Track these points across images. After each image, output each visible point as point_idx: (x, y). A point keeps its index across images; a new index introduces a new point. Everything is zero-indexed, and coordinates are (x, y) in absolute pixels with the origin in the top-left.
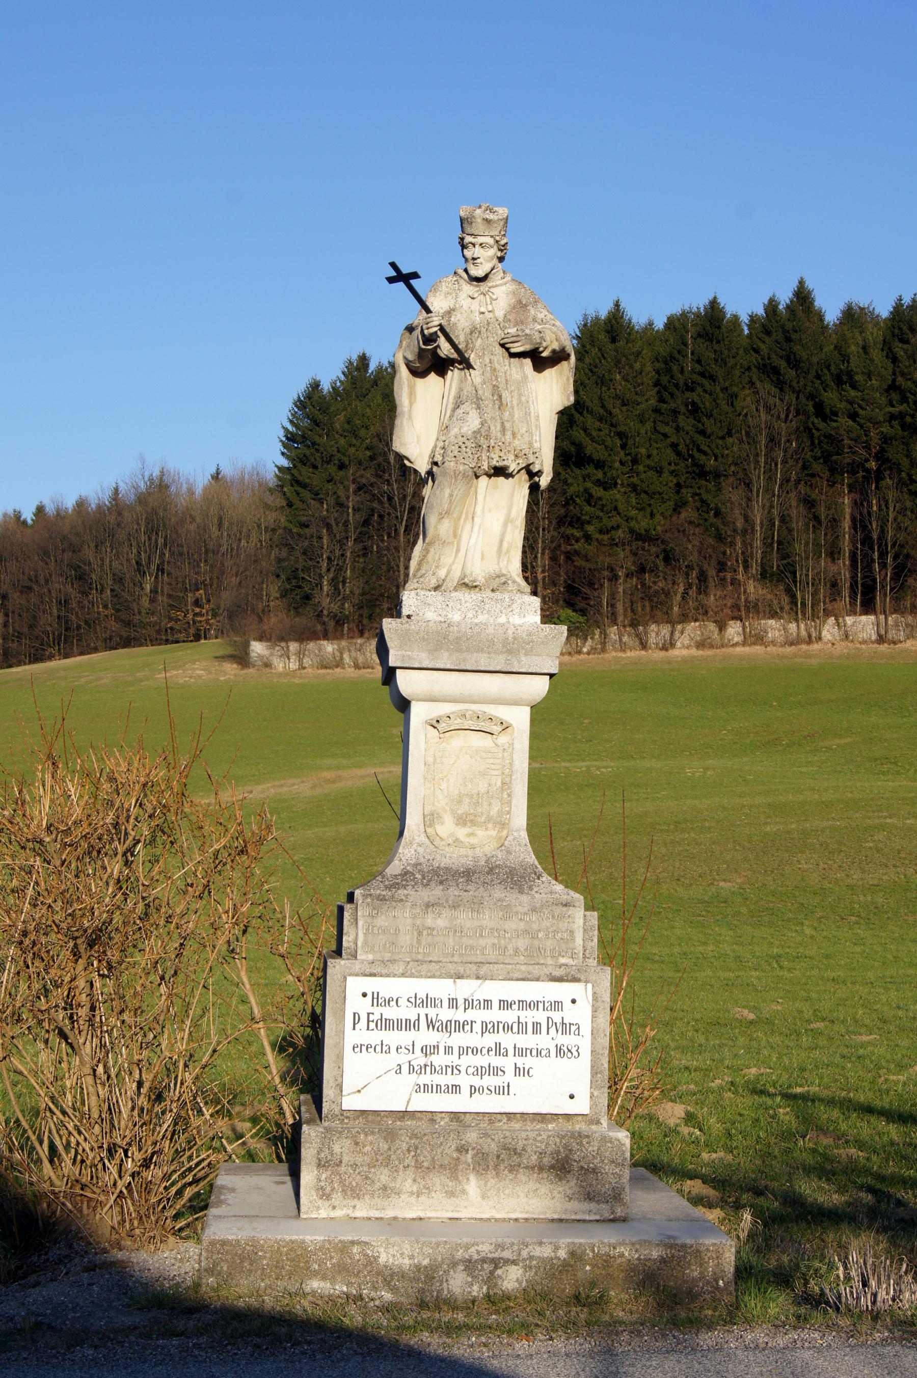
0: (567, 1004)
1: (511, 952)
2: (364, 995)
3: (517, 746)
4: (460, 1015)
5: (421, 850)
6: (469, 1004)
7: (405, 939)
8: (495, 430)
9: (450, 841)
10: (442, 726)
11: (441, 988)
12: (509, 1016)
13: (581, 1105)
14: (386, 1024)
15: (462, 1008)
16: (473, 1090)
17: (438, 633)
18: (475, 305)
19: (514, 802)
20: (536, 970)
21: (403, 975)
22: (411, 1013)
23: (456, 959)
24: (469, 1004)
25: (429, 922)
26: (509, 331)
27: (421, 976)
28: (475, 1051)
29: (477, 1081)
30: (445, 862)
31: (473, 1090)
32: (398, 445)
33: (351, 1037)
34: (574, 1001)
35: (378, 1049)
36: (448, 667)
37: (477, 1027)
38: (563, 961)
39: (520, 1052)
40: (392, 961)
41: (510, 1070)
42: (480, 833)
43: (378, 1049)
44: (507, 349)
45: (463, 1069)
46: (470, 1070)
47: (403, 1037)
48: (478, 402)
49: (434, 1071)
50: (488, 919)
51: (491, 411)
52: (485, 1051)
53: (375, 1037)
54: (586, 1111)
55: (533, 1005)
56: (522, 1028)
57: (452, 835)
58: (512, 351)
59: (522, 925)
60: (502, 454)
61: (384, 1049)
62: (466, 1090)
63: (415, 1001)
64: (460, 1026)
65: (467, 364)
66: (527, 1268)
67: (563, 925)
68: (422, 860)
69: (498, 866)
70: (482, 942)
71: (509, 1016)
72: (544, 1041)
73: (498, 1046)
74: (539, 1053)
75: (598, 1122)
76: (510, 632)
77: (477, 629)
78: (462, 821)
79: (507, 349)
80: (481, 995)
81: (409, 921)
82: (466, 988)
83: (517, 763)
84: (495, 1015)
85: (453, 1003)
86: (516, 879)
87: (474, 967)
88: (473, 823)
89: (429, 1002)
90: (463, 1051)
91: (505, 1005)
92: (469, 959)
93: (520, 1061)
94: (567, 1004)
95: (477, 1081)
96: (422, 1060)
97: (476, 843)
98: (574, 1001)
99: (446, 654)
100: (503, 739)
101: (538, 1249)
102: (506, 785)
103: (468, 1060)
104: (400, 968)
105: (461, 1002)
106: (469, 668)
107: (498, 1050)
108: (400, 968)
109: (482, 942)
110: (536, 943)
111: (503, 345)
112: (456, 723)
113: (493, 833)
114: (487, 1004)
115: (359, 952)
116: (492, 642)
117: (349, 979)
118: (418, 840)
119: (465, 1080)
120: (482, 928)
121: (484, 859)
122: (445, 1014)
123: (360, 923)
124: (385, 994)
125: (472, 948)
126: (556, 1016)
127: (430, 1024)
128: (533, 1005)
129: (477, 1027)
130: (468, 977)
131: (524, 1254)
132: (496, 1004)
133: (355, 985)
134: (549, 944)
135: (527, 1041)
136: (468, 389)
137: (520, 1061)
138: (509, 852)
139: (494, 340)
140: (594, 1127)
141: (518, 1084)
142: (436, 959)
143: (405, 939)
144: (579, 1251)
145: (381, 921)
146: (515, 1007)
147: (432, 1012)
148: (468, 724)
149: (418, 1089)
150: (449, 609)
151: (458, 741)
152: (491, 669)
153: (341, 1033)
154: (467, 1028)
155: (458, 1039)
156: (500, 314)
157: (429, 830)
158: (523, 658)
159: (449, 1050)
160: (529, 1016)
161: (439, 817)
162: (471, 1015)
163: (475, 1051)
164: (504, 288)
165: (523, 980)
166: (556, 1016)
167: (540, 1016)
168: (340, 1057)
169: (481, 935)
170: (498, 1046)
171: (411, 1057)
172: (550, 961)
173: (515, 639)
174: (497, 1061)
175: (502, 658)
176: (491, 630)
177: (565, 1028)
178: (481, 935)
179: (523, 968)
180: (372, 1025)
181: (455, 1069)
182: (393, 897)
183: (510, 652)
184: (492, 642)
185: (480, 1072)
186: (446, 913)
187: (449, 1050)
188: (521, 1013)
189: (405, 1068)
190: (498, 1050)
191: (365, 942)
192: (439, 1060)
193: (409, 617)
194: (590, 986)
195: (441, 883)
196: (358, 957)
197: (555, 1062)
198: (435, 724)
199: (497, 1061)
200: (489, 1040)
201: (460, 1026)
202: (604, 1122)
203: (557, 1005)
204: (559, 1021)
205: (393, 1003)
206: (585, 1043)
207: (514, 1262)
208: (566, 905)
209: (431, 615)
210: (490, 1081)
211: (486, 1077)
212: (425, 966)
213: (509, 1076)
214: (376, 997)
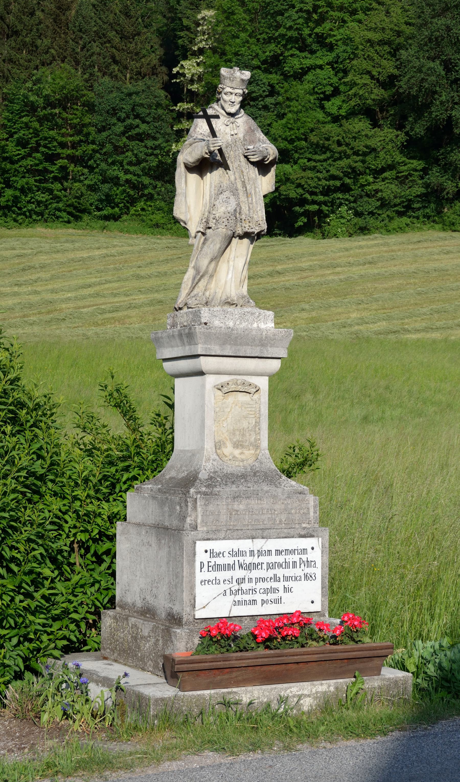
0: (309, 550)
1: (278, 522)
2: (206, 551)
3: (263, 400)
4: (256, 560)
5: (215, 463)
6: (260, 553)
7: (223, 518)
8: (245, 208)
9: (231, 457)
10: (225, 389)
11: (245, 545)
12: (280, 559)
13: (317, 607)
14: (218, 568)
15: (256, 556)
16: (263, 602)
17: (226, 334)
18: (228, 130)
19: (262, 433)
20: (292, 532)
21: (224, 539)
22: (229, 560)
23: (250, 527)
24: (260, 553)
25: (236, 507)
26: (249, 147)
27: (234, 539)
28: (263, 580)
29: (265, 597)
30: (230, 470)
31: (263, 602)
32: (178, 213)
33: (199, 576)
34: (313, 548)
35: (214, 582)
36: (230, 354)
37: (265, 566)
38: (304, 525)
39: (287, 579)
40: (218, 531)
41: (281, 589)
42: (246, 452)
43: (214, 582)
44: (248, 159)
45: (258, 591)
46: (262, 591)
47: (227, 575)
48: (235, 192)
49: (243, 593)
50: (266, 503)
51: (243, 198)
52: (269, 579)
53: (211, 576)
54: (319, 610)
55: (292, 552)
56: (286, 565)
57: (231, 454)
58: (252, 160)
59: (283, 506)
60: (251, 224)
61: (217, 582)
62: (259, 602)
63: (233, 553)
64: (256, 566)
65: (227, 168)
66: (315, 698)
67: (304, 506)
68: (217, 469)
69: (258, 471)
70: (263, 517)
71: (280, 559)
72: (298, 572)
73: (275, 575)
74: (296, 579)
75: (324, 615)
76: (264, 334)
77: (247, 332)
78: (237, 445)
79: (248, 159)
80: (266, 548)
81: (225, 507)
82: (259, 544)
83: (262, 410)
84: (273, 558)
85: (252, 553)
86: (267, 477)
87: (260, 532)
88: (242, 446)
89: (240, 553)
90: (258, 580)
91: (279, 552)
92: (257, 527)
93: (286, 584)
94: (309, 550)
95: (265, 597)
96: (237, 587)
97: (238, 458)
98: (313, 548)
99: (229, 347)
100: (256, 396)
101: (320, 687)
102: (258, 423)
103: (261, 585)
104: (222, 535)
105: (256, 552)
106: (241, 355)
107: (276, 579)
108: (222, 535)
109: (263, 517)
110: (290, 515)
111: (246, 157)
112: (233, 387)
113: (252, 452)
114: (269, 552)
115: (199, 526)
116: (254, 340)
117: (198, 543)
118: (212, 457)
119: (259, 597)
120: (262, 509)
121: (249, 467)
122: (248, 560)
123: (199, 509)
124: (217, 550)
125: (258, 520)
126: (304, 557)
127: (241, 566)
128: (292, 552)
129: (265, 566)
130: (258, 538)
131: (314, 691)
132: (274, 552)
133: (201, 546)
134: (297, 517)
135: (290, 572)
136: (225, 183)
137: (286, 584)
138: (261, 463)
139: (241, 151)
140: (322, 618)
141: (286, 597)
142: (239, 528)
143: (223, 518)
144: (340, 686)
145: (211, 508)
146: (283, 553)
147: (241, 559)
148: (240, 388)
149: (236, 603)
150: (226, 319)
151: (231, 398)
152: (253, 355)
153: (192, 574)
154: (259, 567)
155: (255, 574)
156: (241, 135)
157: (218, 451)
158: (269, 349)
159: (250, 580)
160: (291, 558)
161: (224, 444)
162: (263, 559)
163: (263, 580)
164: (241, 119)
165: (286, 537)
166: (304, 557)
167: (296, 558)
168: (192, 587)
169: (263, 513)
170: (275, 575)
171: (231, 585)
172: (297, 526)
173: (266, 337)
174: (275, 585)
175: (258, 348)
176: (254, 333)
177: (309, 563)
178: (263, 513)
179: (286, 531)
180: (210, 569)
181: (254, 591)
182: (211, 492)
183: (262, 345)
184: (254, 340)
185: (266, 591)
186: (245, 502)
187: (250, 580)
188: (287, 557)
189: (228, 592)
190: (276, 579)
191: (203, 521)
192: (245, 586)
193: (206, 324)
194: (320, 539)
195: (233, 483)
196: (199, 529)
197: (304, 583)
198: (220, 388)
199: (275, 585)
200: (271, 573)
201: (256, 566)
202: (327, 615)
203: (304, 551)
204: (305, 560)
205: (221, 555)
206: (318, 571)
207: (309, 696)
208: (300, 493)
209: (217, 323)
210: (272, 596)
211: (269, 594)
212: (235, 533)
213: (281, 593)
214: (212, 552)
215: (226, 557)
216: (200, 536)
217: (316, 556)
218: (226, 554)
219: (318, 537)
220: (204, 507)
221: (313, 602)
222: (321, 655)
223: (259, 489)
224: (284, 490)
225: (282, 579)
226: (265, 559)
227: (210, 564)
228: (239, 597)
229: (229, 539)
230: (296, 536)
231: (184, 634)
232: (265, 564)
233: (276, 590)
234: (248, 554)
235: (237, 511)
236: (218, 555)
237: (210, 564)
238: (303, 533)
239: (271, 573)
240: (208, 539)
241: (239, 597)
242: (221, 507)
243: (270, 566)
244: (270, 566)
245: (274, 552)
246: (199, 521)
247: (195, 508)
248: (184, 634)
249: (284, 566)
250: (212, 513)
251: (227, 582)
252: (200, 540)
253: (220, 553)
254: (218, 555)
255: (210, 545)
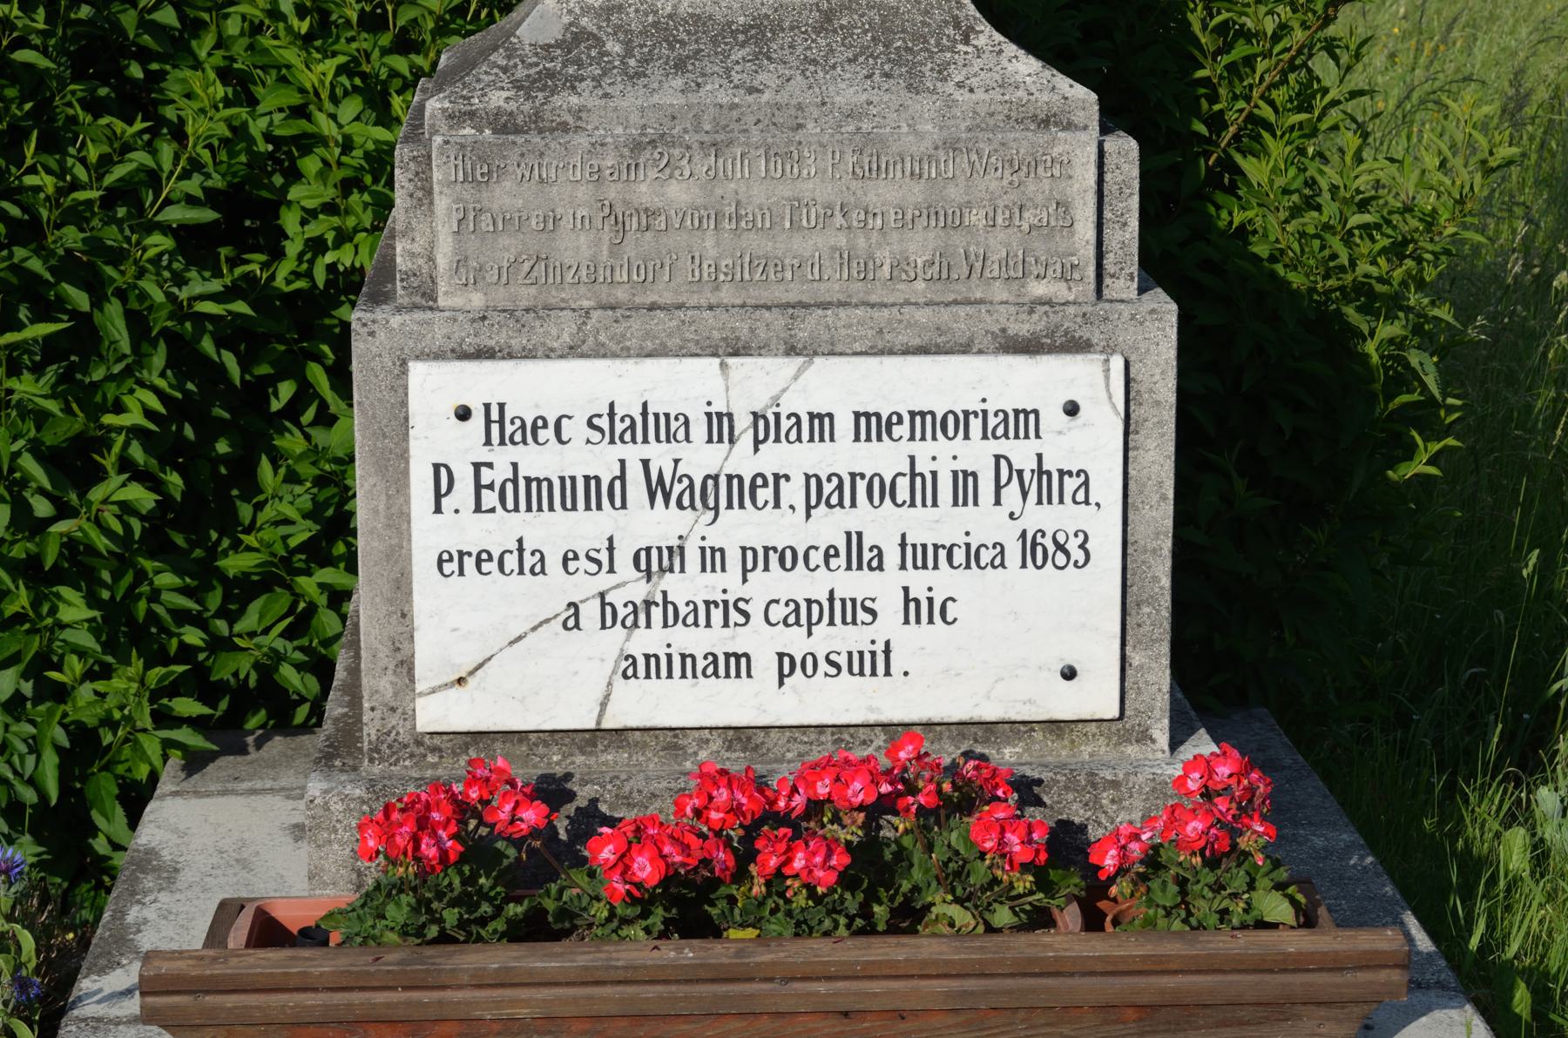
4: (743, 460)
6: (766, 427)
11: (685, 385)
13: (1096, 696)
14: (531, 493)
15: (746, 441)
16: (787, 666)
20: (960, 321)
21: (574, 351)
24: (766, 427)
28: (788, 558)
29: (796, 641)
31: (787, 666)
33: (429, 532)
34: (1072, 409)
35: (511, 562)
37: (793, 492)
38: (1039, 289)
39: (919, 556)
43: (511, 562)
45: (756, 610)
46: (777, 613)
47: (584, 528)
49: (672, 616)
52: (816, 558)
53: (498, 531)
55: (954, 424)
56: (922, 488)
62: (765, 666)
63: (610, 426)
64: (743, 491)
71: (885, 458)
72: (987, 523)
73: (854, 540)
74: (973, 557)
80: (799, 402)
82: (757, 382)
84: (844, 455)
85: (720, 426)
87: (777, 320)
90: (754, 559)
91: (872, 425)
93: (919, 582)
94: (1053, 417)
95: (796, 641)
96: (639, 591)
98: (1072, 409)
103: (769, 584)
105: (743, 422)
107: (857, 553)
108: (564, 329)
110: (958, 240)
114: (821, 425)
115: (442, 287)
117: (418, 371)
119: (762, 643)
122: (701, 458)
123: (442, 203)
124: (522, 408)
126: (1022, 454)
127: (657, 489)
128: (954, 424)
129: (793, 492)
132: (844, 425)
133: (434, 388)
135: (939, 524)
137: (919, 582)
141: (911, 643)
142: (667, 298)
145: (505, 195)
146: (901, 431)
147: (661, 456)
149: (629, 667)
154: (765, 494)
155: (738, 528)
159: (713, 558)
163: (788, 558)
166: (1022, 454)
167: (976, 454)
168: (402, 586)
170: (854, 540)
171: (604, 581)
172: (999, 292)
174: (852, 584)
177: (1046, 483)
179: (923, 316)
180: (489, 498)
181: (734, 610)
182: (537, 116)
185: (803, 614)
187: (713, 558)
188: (923, 450)
190: (857, 553)
191: (460, 263)
192: (686, 586)
195: (680, 66)
196: (441, 302)
199: (852, 584)
200: (829, 527)
201: (743, 491)
203: (1023, 421)
204: (1028, 465)
205: (547, 434)
208: (1044, 123)
211: (821, 630)
212: (636, 324)
213: (889, 623)
215: (578, 442)
216: (439, 331)
217: (1093, 445)
218: (575, 429)
219: (1109, 350)
220: (468, 193)
221: (1069, 674)
222: (971, 984)
223: (808, 98)
224: (950, 102)
225: (892, 557)
226: (795, 459)
227: (487, 476)
228: (648, 640)
229: (600, 352)
230: (982, 341)
231: (337, 807)
232: (798, 482)
233: (857, 611)
234: (699, 430)
235: (652, 213)
236: (531, 431)
237: (487, 476)
238: (1023, 328)
239: (829, 527)
240: (484, 354)
241: (648, 640)
242: (559, 193)
243: (823, 493)
244: (823, 493)
245: (844, 425)
246: (443, 262)
247: (426, 192)
248: (337, 807)
249: (903, 493)
250: (511, 223)
251: (584, 563)
252: (438, 356)
253: (539, 423)
254: (531, 431)
255: (483, 382)
